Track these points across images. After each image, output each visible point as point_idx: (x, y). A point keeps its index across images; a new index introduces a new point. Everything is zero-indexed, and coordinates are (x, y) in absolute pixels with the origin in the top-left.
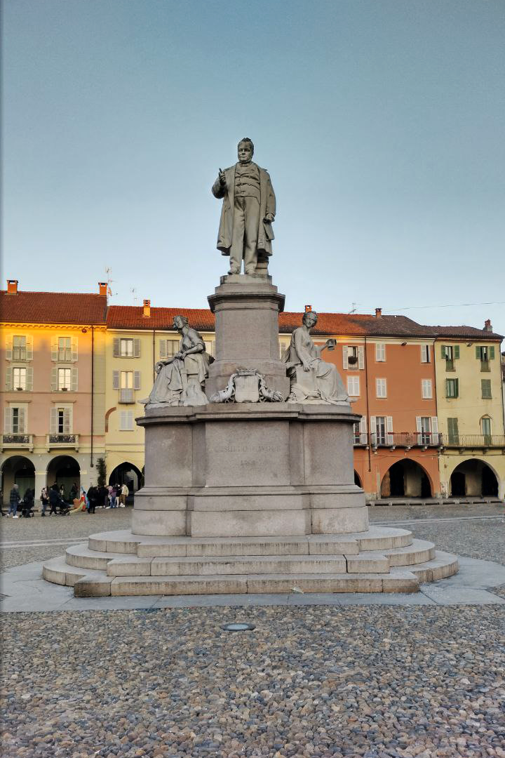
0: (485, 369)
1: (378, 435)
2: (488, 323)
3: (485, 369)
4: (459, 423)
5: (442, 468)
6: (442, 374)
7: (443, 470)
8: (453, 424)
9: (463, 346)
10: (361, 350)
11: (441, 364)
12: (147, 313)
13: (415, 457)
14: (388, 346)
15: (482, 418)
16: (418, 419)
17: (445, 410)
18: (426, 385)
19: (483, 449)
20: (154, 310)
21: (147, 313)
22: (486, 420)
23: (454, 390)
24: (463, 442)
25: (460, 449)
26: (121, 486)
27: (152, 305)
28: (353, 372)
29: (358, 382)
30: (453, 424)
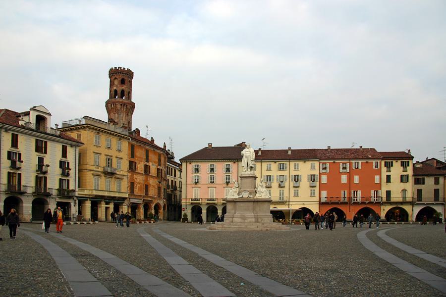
0: (405, 171)
1: (374, 197)
2: (409, 151)
3: (405, 171)
4: (310, 195)
5: (382, 210)
6: (384, 173)
7: (350, 213)
8: (388, 193)
9: (394, 162)
10: (348, 165)
11: (384, 169)
12: (290, 153)
13: (370, 206)
14: (362, 162)
15: (403, 190)
16: (372, 192)
17: (385, 188)
18: (377, 178)
19: (402, 203)
20: (292, 151)
21: (290, 153)
22: (404, 191)
23: (388, 179)
24: (392, 200)
25: (391, 203)
26: (332, 214)
27: (292, 149)
28: (344, 173)
29: (346, 177)
30: (388, 193)
